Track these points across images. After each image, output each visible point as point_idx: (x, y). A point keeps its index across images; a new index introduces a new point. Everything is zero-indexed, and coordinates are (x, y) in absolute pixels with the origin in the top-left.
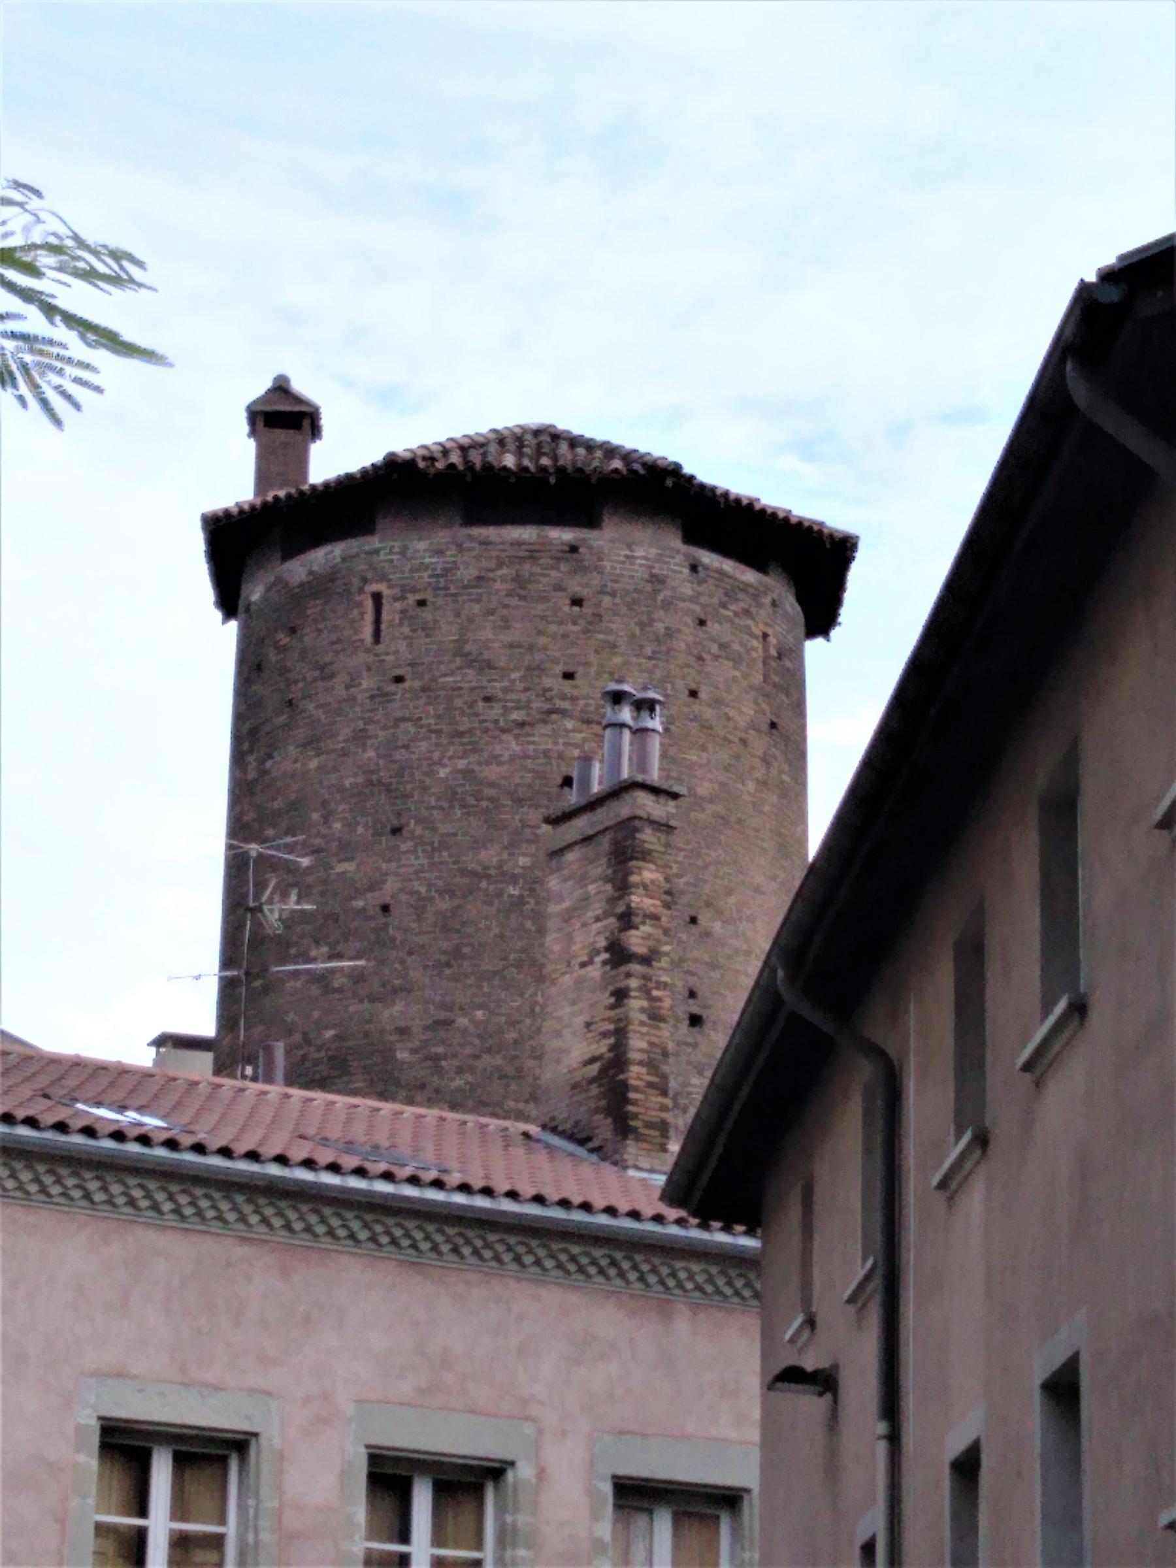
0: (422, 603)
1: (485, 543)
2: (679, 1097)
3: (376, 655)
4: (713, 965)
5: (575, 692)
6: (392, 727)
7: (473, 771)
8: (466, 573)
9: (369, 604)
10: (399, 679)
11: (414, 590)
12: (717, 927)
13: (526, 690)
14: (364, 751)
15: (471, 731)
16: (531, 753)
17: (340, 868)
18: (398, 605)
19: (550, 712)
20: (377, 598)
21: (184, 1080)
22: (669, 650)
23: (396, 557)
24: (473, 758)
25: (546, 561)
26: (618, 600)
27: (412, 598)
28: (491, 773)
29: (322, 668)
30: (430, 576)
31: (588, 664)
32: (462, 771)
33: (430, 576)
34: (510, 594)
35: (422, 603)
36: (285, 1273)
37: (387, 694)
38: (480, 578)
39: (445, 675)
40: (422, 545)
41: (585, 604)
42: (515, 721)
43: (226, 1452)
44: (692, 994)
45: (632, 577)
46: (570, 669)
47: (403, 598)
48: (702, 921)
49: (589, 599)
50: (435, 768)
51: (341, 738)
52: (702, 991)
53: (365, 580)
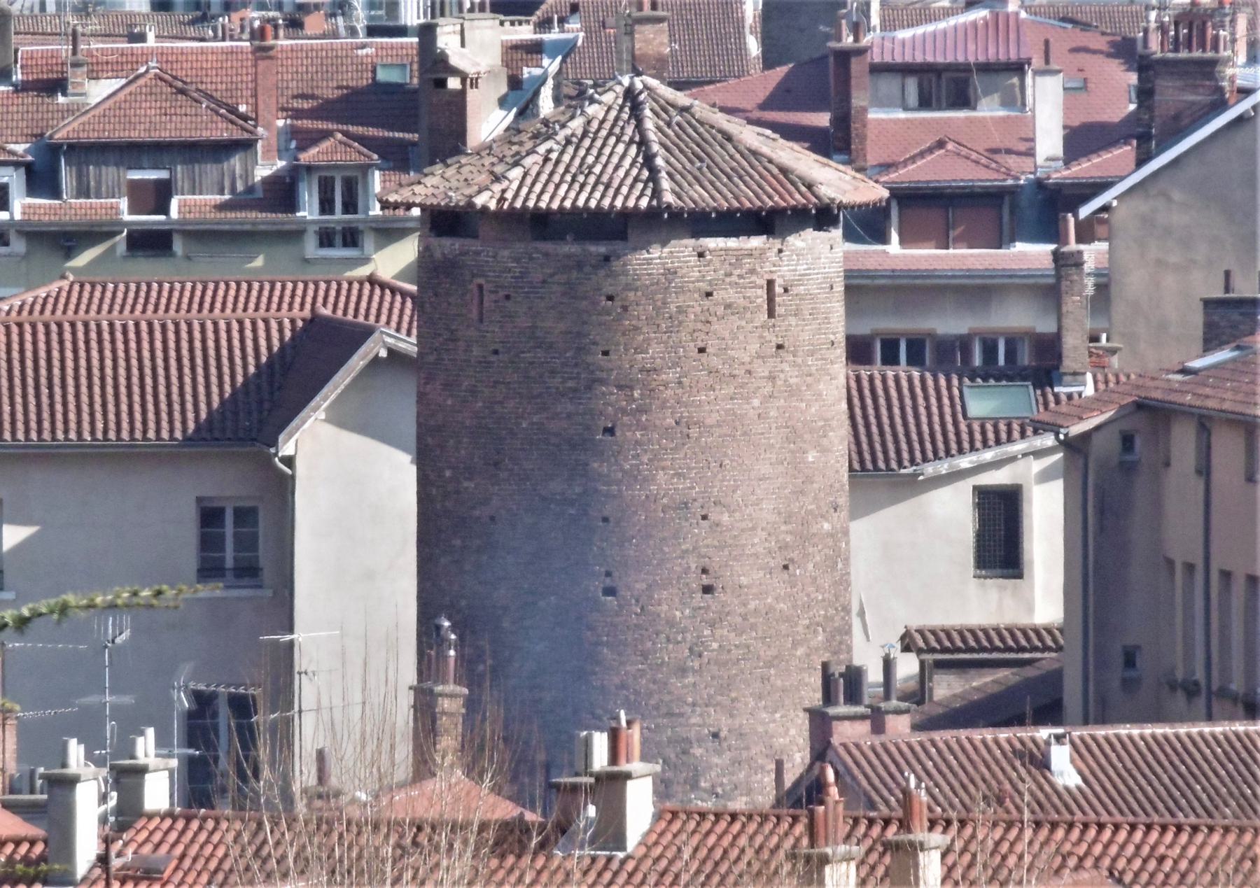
0: (508, 297)
1: (546, 255)
2: (882, 694)
3: (480, 331)
4: (721, 548)
5: (610, 366)
6: (492, 387)
7: (543, 424)
8: (537, 276)
9: (476, 290)
10: (496, 352)
11: (503, 287)
12: (725, 518)
13: (576, 365)
14: (476, 402)
15: (540, 395)
16: (44, 610)
17: (466, 484)
18: (493, 297)
19: (594, 381)
20: (480, 287)
21: (423, 208)
22: (680, 323)
23: (490, 259)
24: (545, 415)
25: (587, 269)
26: (639, 293)
27: (502, 293)
28: (553, 426)
29: (452, 332)
30: (512, 277)
31: (618, 344)
32: (536, 423)
33: (512, 277)
34: (564, 294)
35: (508, 297)
36: (412, 462)
37: (489, 362)
38: (544, 282)
39: (523, 352)
40: (506, 253)
41: (616, 299)
42: (570, 388)
43: (394, 281)
44: (704, 571)
45: (649, 275)
46: (606, 348)
47: (496, 292)
48: (712, 517)
49: (618, 295)
50: (519, 420)
51: (463, 388)
52: (714, 566)
53: (474, 276)
